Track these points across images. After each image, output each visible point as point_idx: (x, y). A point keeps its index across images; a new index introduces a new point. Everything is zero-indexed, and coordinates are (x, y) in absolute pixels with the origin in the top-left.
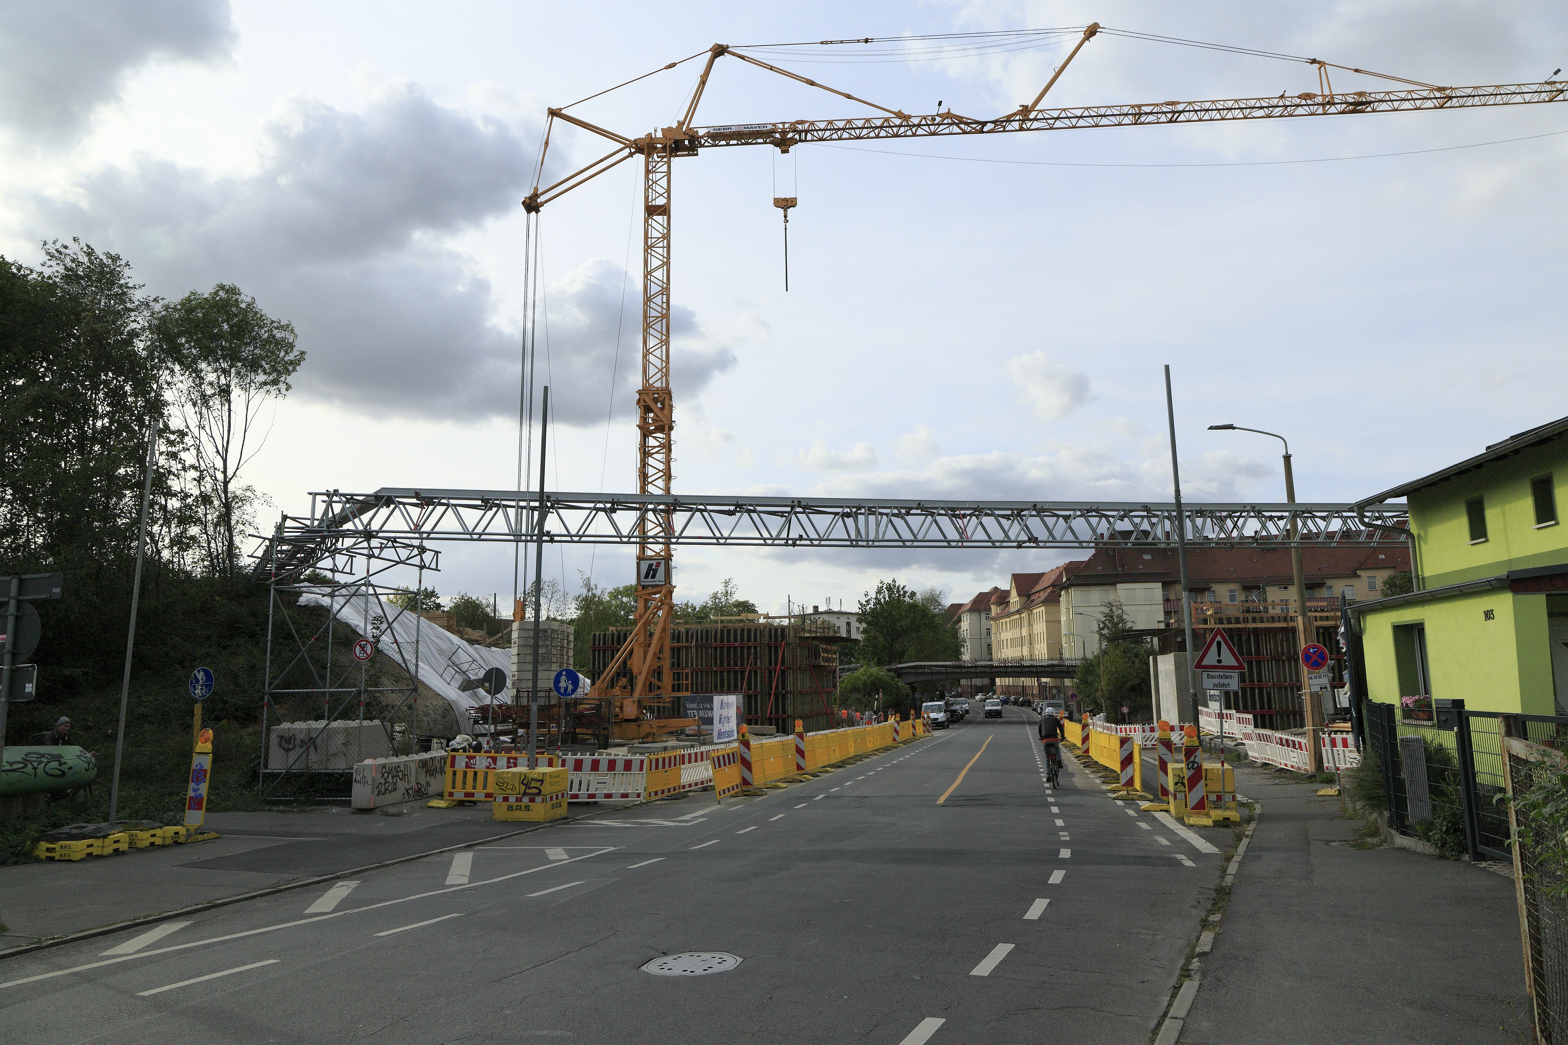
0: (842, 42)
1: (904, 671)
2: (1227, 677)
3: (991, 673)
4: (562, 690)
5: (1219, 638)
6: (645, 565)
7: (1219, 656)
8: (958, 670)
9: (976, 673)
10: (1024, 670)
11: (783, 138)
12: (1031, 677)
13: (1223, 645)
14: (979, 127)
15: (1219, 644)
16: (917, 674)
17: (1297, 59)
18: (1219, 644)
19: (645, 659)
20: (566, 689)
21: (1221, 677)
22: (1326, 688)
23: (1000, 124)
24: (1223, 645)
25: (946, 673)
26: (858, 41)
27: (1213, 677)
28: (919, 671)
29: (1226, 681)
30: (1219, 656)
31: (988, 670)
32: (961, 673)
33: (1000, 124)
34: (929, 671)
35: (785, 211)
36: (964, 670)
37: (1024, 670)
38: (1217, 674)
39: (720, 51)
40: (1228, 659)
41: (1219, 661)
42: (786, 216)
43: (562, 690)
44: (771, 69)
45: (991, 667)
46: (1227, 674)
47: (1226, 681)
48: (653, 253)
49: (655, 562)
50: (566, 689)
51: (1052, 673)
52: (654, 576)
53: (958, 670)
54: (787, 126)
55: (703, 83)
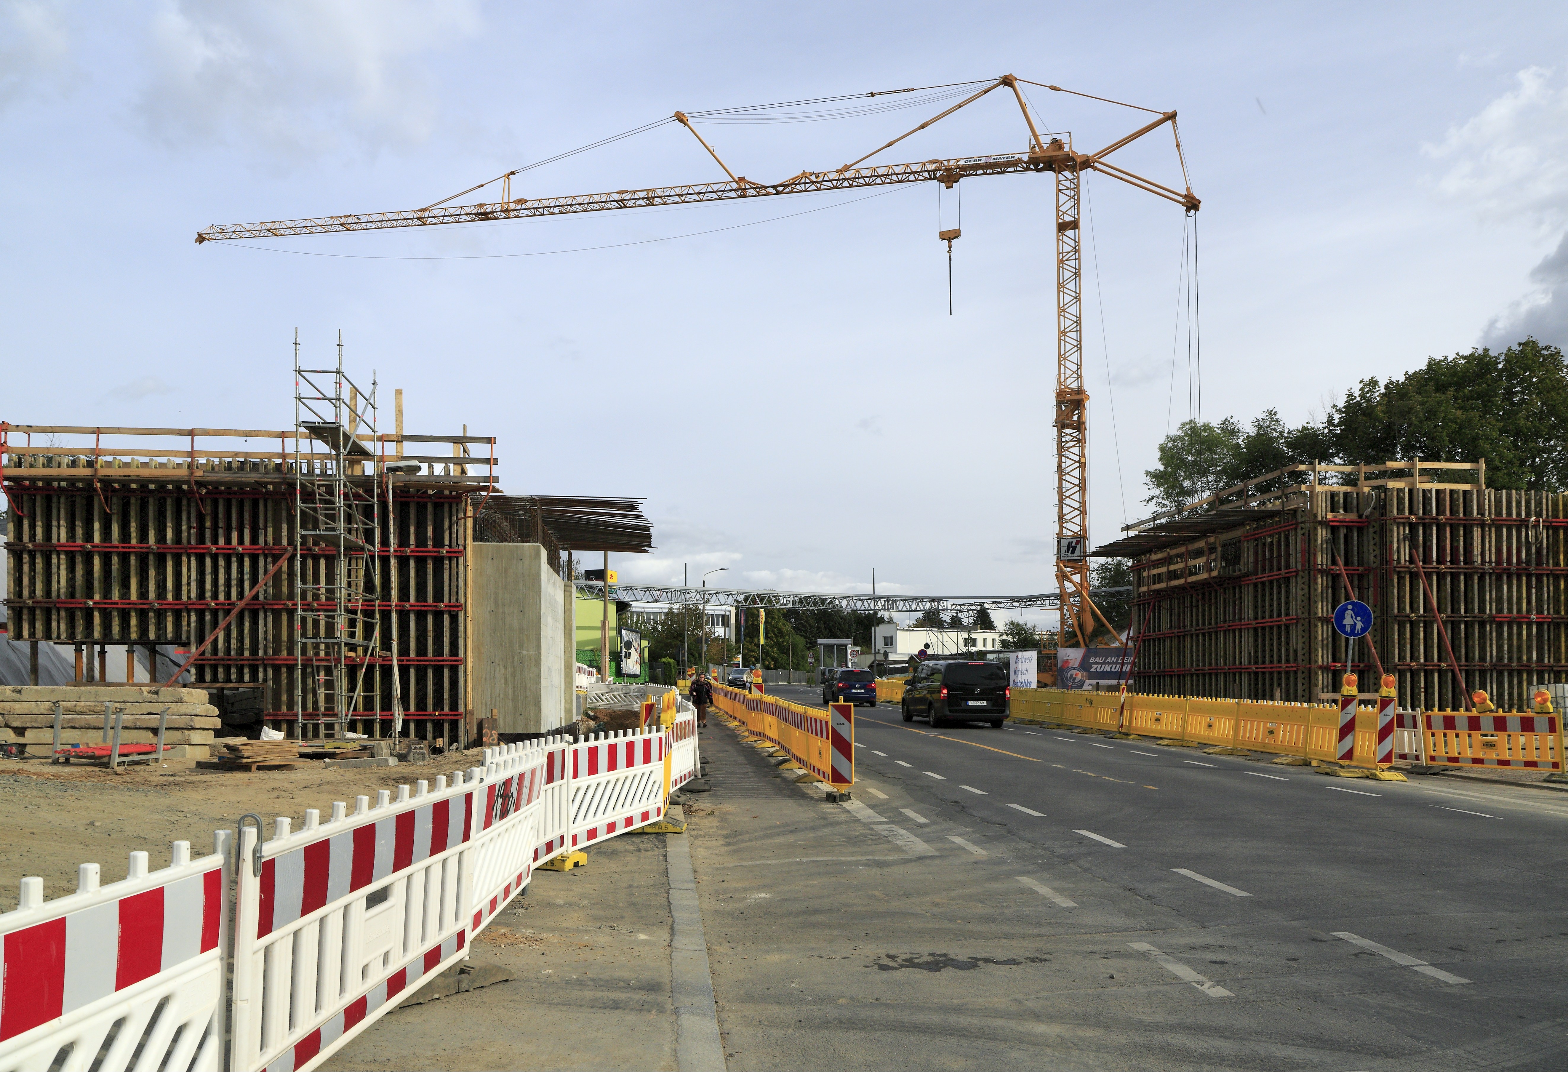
0: (895, 92)
4: (1348, 629)
6: (1064, 543)
11: (949, 175)
14: (761, 190)
17: (525, 169)
20: (1354, 626)
23: (779, 189)
26: (880, 94)
33: (779, 189)
35: (950, 242)
39: (1007, 81)
42: (950, 247)
43: (1348, 629)
44: (960, 107)
48: (1065, 266)
49: (1074, 541)
50: (1354, 626)
52: (1073, 552)
54: (951, 163)
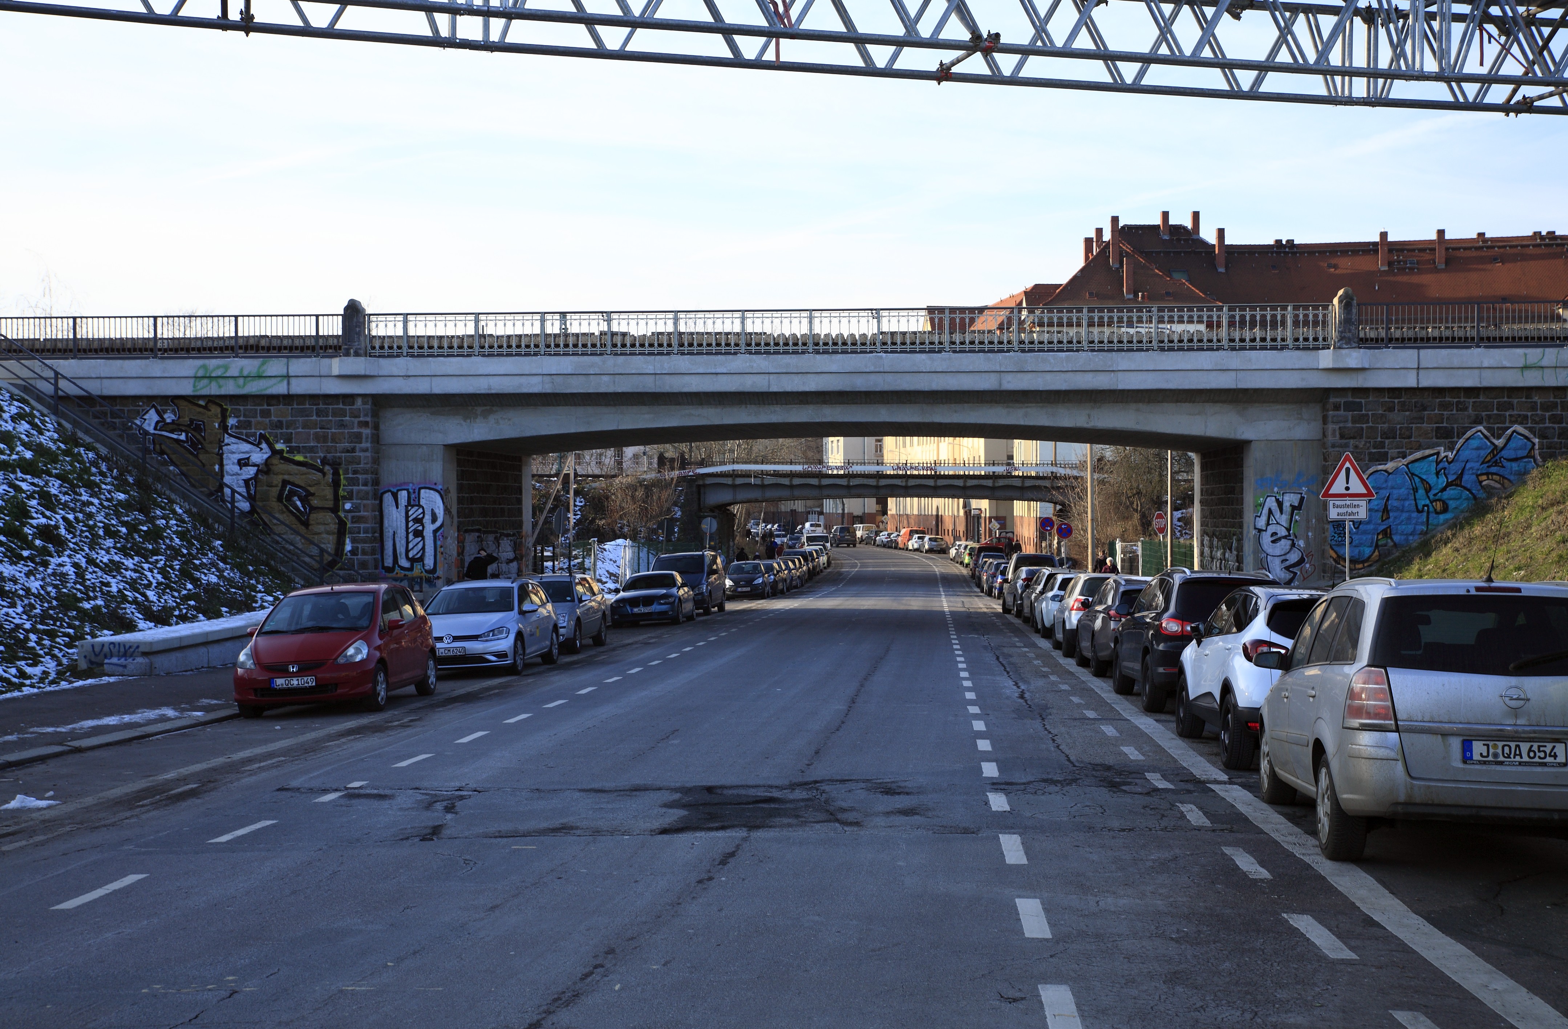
1: (709, 481)
3: (877, 487)
5: (1348, 465)
8: (814, 481)
9: (848, 487)
10: (941, 482)
12: (953, 497)
13: (1352, 472)
15: (1348, 470)
16: (734, 486)
18: (1348, 470)
22: (1239, 569)
24: (1352, 472)
25: (792, 487)
28: (739, 481)
29: (1355, 510)
31: (872, 482)
34: (759, 482)
36: (825, 482)
37: (941, 482)
40: (1357, 486)
41: (1347, 489)
45: (879, 476)
46: (1355, 503)
47: (1355, 510)
51: (993, 488)
53: (814, 481)
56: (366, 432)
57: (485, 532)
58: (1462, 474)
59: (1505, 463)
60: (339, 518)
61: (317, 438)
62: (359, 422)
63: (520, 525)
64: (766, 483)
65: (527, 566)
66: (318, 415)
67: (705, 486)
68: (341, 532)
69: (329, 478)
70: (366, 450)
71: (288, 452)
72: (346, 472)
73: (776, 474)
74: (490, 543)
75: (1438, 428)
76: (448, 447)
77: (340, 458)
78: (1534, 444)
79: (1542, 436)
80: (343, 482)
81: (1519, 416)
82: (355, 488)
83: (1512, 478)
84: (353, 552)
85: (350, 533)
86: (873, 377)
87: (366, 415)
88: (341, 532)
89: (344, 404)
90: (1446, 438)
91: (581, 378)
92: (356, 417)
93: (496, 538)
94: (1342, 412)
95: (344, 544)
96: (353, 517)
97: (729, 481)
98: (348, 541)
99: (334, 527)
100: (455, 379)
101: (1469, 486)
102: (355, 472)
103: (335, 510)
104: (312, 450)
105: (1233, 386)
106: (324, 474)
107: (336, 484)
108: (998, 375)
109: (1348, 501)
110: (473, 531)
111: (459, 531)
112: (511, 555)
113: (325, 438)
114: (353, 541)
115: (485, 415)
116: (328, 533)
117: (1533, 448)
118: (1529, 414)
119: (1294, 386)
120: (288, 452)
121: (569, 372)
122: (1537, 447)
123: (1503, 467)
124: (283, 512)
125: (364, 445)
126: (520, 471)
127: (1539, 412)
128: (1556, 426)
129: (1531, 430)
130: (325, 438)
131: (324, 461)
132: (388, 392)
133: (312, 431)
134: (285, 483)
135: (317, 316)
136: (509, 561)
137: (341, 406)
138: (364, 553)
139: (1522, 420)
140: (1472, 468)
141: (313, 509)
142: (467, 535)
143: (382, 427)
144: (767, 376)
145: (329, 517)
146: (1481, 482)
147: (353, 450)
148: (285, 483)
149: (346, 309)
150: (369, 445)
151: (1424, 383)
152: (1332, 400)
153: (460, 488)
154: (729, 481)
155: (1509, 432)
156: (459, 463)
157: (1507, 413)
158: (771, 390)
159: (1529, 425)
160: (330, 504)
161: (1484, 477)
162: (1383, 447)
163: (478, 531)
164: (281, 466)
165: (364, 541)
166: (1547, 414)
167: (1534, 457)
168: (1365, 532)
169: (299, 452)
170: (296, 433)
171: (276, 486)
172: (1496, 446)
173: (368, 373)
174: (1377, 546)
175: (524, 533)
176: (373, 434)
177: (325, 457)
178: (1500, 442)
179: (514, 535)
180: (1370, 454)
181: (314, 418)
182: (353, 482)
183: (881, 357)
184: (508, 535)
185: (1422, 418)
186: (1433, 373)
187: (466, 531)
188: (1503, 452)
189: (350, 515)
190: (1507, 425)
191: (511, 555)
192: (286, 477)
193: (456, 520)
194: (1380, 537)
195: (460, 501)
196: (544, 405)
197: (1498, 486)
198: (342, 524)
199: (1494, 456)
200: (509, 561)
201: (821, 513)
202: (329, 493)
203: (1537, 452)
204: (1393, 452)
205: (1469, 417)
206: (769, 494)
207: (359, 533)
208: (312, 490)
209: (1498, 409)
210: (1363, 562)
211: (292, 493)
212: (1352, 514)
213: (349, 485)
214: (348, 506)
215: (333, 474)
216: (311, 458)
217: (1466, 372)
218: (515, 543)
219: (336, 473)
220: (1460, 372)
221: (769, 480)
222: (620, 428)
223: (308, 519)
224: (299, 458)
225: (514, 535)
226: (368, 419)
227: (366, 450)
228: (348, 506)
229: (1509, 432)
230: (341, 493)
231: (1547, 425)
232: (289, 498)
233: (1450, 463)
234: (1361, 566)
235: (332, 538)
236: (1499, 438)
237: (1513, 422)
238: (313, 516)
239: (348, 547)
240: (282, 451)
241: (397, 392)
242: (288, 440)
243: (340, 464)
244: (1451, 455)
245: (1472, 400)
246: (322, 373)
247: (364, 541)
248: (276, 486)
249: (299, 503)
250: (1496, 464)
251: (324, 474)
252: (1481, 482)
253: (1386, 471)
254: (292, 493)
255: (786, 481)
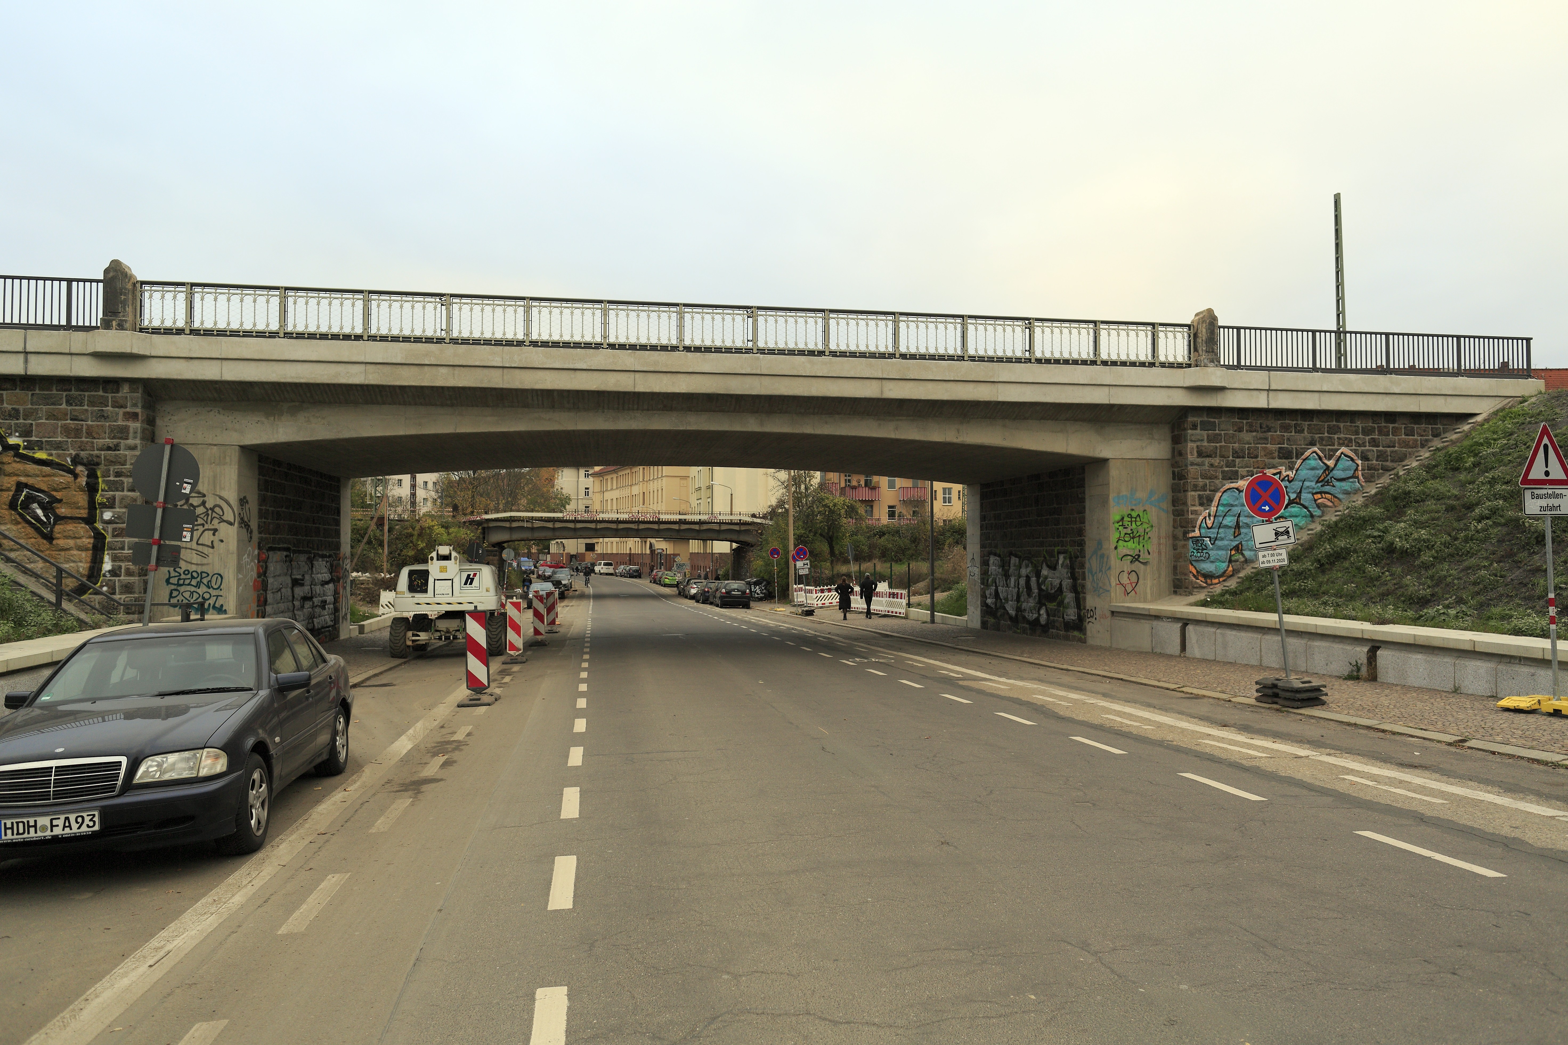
1: (492, 525)
2: (1557, 496)
5: (1546, 441)
7: (1547, 466)
15: (1546, 446)
18: (1546, 446)
19: (162, 695)
21: (1549, 496)
27: (1539, 497)
28: (515, 525)
30: (1547, 466)
31: (614, 526)
32: (554, 529)
34: (529, 525)
38: (1545, 491)
41: (1547, 473)
46: (1557, 491)
55: (191, 358)
56: (135, 426)
57: (295, 552)
58: (1300, 492)
59: (1337, 484)
60: (95, 530)
61: (67, 431)
62: (125, 414)
63: (337, 546)
64: (535, 526)
65: (345, 588)
66: (68, 403)
67: (489, 528)
68: (98, 547)
69: (83, 481)
70: (133, 448)
71: (25, 448)
72: (106, 474)
73: (541, 519)
74: (302, 564)
75: (1280, 448)
76: (244, 448)
77: (98, 457)
78: (1358, 465)
79: (1365, 458)
80: (101, 486)
81: (1346, 438)
82: (118, 494)
83: (1341, 496)
84: (114, 572)
85: (110, 549)
86: (748, 379)
87: (135, 405)
88: (98, 547)
89: (105, 391)
90: (1286, 458)
91: (414, 369)
92: (121, 407)
93: (309, 558)
94: (1198, 431)
95: (101, 562)
96: (114, 530)
97: (507, 525)
98: (106, 558)
99: (88, 542)
100: (253, 364)
101: (1306, 504)
102: (118, 474)
103: (90, 520)
104: (58, 446)
105: (1106, 402)
106: (76, 476)
107: (92, 489)
108: (879, 382)
109: (1548, 490)
110: (279, 549)
111: (259, 548)
112: (327, 576)
113: (77, 432)
114: (114, 559)
115: (294, 411)
116: (80, 548)
117: (1357, 469)
118: (1353, 437)
119: (1161, 404)
120: (25, 448)
121: (399, 361)
122: (1360, 468)
123: (1334, 486)
124: (18, 523)
125: (130, 442)
126: (339, 492)
127: (1361, 436)
128: (1375, 449)
129: (1355, 452)
130: (77, 432)
131: (76, 460)
132: (163, 376)
133: (60, 423)
134: (20, 486)
135: (70, 281)
136: (325, 583)
137: (101, 393)
138: (129, 573)
139: (1347, 443)
140: (1308, 487)
141: (59, 519)
142: (271, 553)
143: (159, 422)
144: (632, 375)
145: (82, 528)
146: (1315, 500)
147: (116, 448)
148: (20, 486)
149: (106, 271)
150: (138, 442)
151: (1274, 405)
152: (1190, 419)
153: (262, 500)
154: (507, 525)
155: (1338, 453)
156: (262, 471)
157: (1336, 436)
158: (637, 390)
159: (1354, 447)
160: (84, 513)
161: (1319, 496)
162: (1234, 466)
163: (287, 549)
164: (14, 465)
165: (127, 559)
166: (1367, 438)
167: (1357, 478)
168: (1220, 548)
169: (41, 449)
170: (38, 425)
171: (8, 490)
172: (1328, 467)
173: (135, 351)
174: (1230, 561)
175: (341, 555)
176: (144, 430)
177: (77, 455)
178: (1331, 463)
179: (330, 556)
180: (1223, 472)
181: (64, 406)
182: (115, 486)
183: (758, 358)
184: (323, 556)
185: (1266, 439)
186: (1281, 395)
187: (271, 549)
188: (1334, 472)
189: (110, 527)
190: (1336, 447)
191: (327, 576)
192: (23, 479)
193: (256, 535)
194: (1233, 552)
195: (262, 514)
196: (366, 403)
197: (1330, 504)
198: (99, 538)
199: (1327, 476)
200: (325, 583)
201: (549, 553)
202: (82, 499)
203: (1360, 473)
204: (1243, 471)
205: (1305, 438)
206: (537, 535)
207: (123, 548)
208: (58, 495)
209: (1328, 433)
210: (1219, 577)
211: (30, 499)
212: (1553, 508)
213: (110, 490)
214: (107, 515)
215: (88, 476)
216: (59, 456)
217: (1308, 394)
218: (332, 565)
219: (92, 475)
220: (1303, 394)
221: (537, 524)
222: (458, 431)
223: (52, 531)
224: (41, 455)
225: (330, 556)
226: (138, 410)
227: (133, 448)
228: (107, 515)
229: (1338, 453)
230: (99, 498)
231: (1367, 448)
232: (26, 505)
233: (1290, 482)
234: (1216, 581)
235: (86, 556)
236: (1329, 459)
237: (1341, 445)
238: (57, 528)
239: (107, 566)
240: (16, 447)
241: (175, 377)
242: (26, 433)
243: (98, 464)
244: (1291, 474)
245: (1307, 423)
246: (73, 351)
247: (127, 559)
248: (8, 490)
249: (39, 512)
250: (1328, 483)
251: (76, 476)
252: (1315, 500)
253: (1237, 489)
254: (30, 499)
255: (550, 525)
